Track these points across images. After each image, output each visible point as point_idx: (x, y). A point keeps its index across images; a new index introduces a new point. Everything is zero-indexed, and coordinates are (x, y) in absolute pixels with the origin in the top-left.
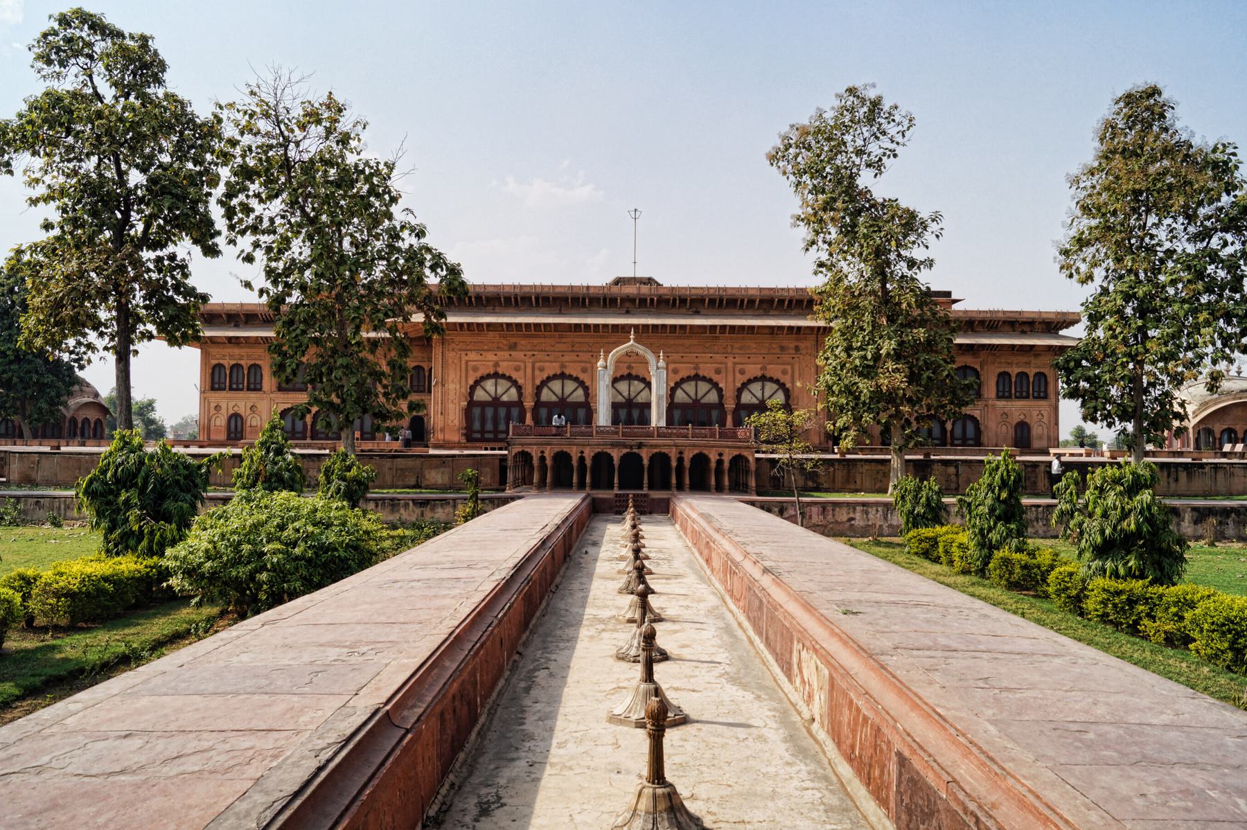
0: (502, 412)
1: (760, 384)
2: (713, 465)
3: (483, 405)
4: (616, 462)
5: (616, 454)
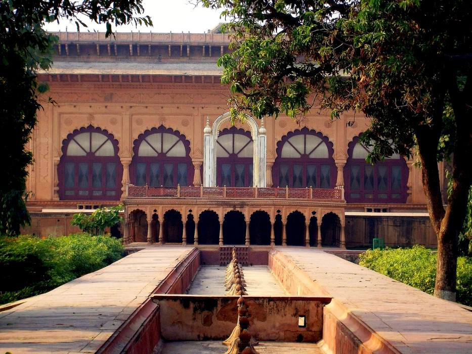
0: (97, 168)
1: (231, 136)
2: (307, 222)
3: (76, 160)
4: (221, 219)
5: (221, 213)
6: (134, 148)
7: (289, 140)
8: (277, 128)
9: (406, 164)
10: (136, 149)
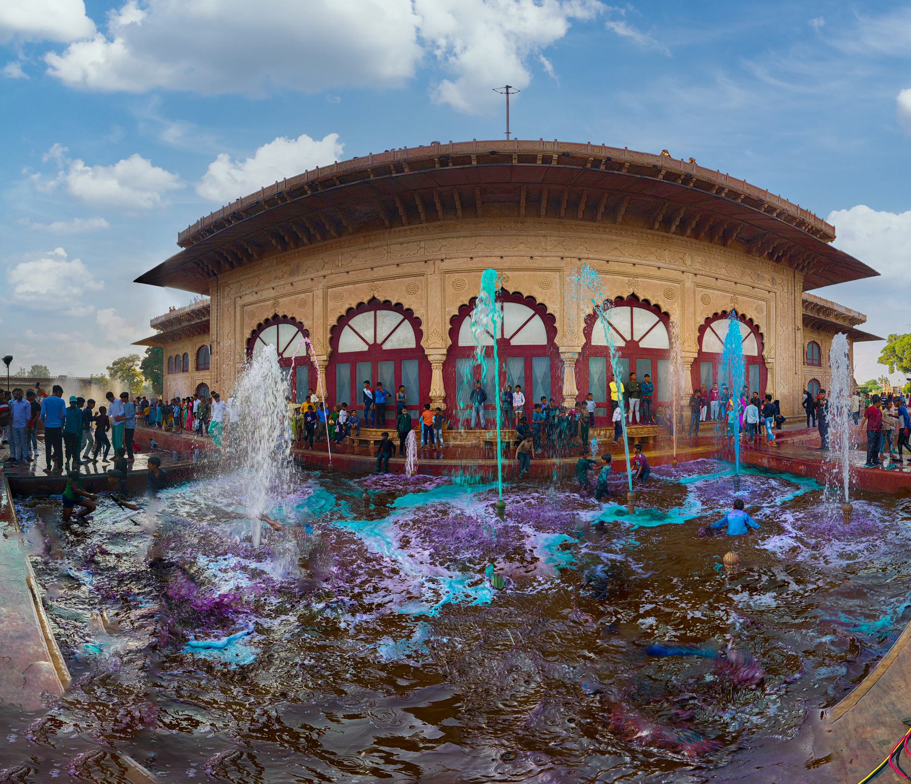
6: (331, 339)
7: (406, 321)
8: (450, 290)
9: (426, 356)
10: (334, 340)
